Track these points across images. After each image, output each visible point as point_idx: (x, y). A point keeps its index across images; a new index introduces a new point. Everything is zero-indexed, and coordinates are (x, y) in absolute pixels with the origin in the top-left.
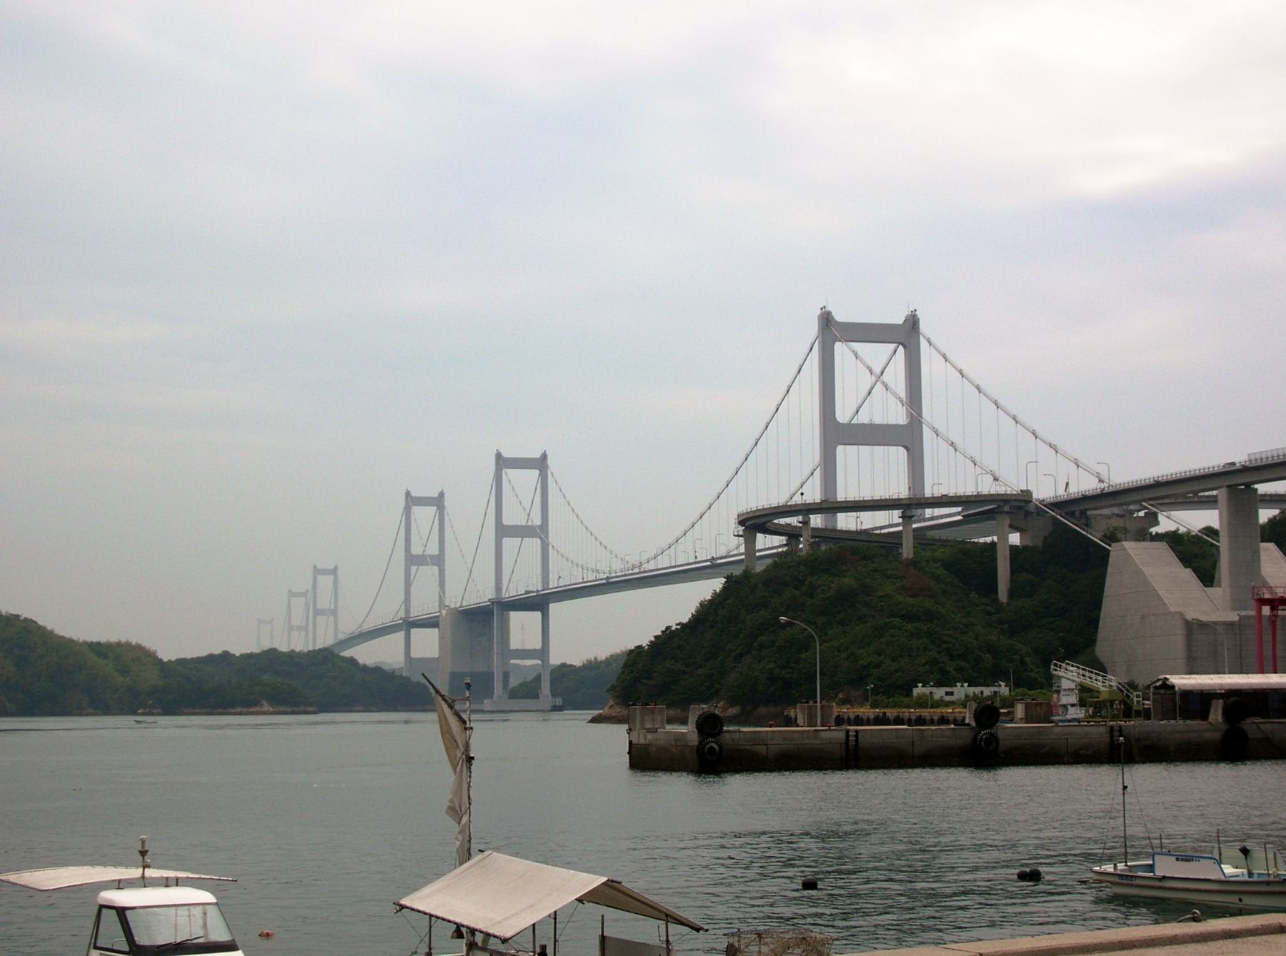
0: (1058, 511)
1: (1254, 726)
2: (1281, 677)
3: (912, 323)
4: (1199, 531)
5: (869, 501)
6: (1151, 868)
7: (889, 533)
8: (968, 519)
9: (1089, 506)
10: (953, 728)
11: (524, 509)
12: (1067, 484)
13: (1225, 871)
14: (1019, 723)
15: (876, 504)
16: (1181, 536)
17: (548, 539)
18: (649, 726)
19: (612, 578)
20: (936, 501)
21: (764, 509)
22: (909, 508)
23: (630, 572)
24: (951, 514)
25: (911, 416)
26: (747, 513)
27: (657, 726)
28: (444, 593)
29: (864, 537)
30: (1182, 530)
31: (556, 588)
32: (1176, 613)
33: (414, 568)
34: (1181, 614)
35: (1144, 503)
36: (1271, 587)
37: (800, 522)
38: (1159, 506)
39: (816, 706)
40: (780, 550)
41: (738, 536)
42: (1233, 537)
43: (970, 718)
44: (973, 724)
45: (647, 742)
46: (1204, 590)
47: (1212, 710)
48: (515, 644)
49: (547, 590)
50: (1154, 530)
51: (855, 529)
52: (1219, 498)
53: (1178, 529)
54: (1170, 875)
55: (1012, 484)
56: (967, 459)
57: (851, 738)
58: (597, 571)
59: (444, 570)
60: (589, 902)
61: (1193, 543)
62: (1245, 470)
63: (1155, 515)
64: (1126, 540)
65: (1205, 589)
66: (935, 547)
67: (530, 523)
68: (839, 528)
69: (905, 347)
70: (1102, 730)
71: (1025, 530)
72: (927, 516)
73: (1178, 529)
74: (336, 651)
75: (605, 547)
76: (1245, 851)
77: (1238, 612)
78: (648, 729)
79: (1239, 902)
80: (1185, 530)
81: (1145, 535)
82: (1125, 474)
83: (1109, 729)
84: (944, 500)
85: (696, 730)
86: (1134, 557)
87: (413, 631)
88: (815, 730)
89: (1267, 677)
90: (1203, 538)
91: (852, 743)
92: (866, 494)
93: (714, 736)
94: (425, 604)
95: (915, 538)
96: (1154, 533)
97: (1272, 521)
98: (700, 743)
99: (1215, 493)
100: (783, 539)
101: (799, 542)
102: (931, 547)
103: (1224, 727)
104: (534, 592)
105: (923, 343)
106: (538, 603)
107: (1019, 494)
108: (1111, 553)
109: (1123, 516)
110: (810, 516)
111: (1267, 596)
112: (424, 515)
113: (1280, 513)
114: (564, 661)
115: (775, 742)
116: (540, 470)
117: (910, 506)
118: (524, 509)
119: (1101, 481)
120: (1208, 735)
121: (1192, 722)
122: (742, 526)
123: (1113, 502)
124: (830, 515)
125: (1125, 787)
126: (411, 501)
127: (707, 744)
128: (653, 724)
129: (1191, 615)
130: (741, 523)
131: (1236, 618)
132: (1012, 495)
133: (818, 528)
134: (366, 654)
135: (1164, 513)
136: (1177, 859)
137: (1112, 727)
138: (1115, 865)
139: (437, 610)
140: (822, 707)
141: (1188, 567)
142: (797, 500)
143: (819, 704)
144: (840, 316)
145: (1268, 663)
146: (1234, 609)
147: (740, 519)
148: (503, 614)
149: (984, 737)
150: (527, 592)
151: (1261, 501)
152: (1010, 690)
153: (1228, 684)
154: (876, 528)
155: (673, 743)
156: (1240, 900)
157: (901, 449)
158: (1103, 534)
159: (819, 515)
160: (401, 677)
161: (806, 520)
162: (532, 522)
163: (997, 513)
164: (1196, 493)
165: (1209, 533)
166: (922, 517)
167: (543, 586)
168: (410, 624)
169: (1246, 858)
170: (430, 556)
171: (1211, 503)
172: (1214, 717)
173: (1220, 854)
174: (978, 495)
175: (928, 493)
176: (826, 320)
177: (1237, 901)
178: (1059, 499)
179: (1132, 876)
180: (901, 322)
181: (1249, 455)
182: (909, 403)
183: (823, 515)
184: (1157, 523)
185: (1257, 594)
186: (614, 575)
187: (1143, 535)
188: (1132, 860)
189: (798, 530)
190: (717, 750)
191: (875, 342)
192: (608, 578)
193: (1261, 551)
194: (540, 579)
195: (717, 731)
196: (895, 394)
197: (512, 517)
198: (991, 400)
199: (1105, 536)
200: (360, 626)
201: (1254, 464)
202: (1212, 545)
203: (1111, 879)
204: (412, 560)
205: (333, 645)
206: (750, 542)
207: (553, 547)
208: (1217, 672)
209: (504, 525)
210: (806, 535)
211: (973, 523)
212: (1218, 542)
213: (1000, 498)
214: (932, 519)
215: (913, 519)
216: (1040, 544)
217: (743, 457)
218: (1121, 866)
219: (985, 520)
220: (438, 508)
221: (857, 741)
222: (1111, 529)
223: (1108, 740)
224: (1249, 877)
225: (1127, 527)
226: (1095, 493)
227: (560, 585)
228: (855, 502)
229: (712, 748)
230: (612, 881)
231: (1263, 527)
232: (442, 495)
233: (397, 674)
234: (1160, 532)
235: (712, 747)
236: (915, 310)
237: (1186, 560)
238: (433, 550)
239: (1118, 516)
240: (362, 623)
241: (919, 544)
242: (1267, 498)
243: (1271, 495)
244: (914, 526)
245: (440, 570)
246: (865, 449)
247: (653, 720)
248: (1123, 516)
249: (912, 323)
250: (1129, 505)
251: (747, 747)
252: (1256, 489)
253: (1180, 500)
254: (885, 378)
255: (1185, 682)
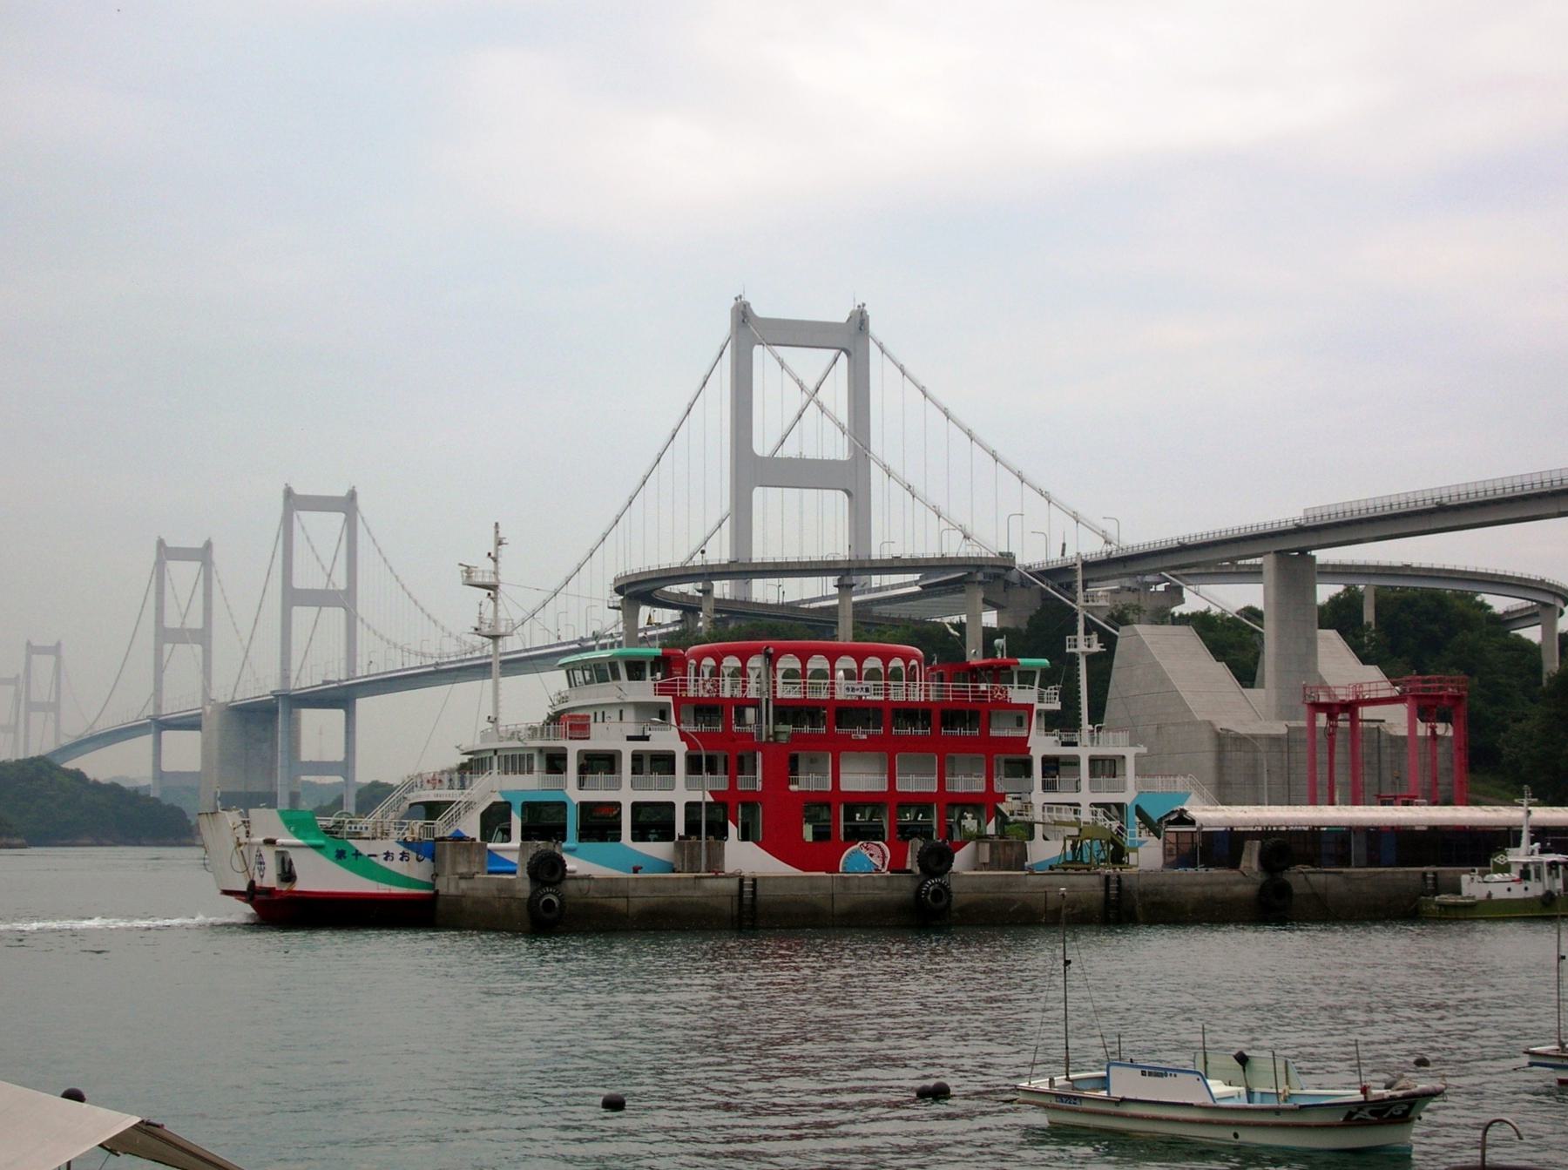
0: (1049, 582)
1: (1302, 878)
2: (1338, 810)
3: (860, 322)
4: (1237, 613)
5: (807, 562)
6: (1104, 1082)
7: (821, 608)
8: (928, 591)
9: (1093, 576)
10: (888, 877)
11: (323, 568)
12: (1064, 545)
13: (1214, 1090)
14: (981, 870)
15: (803, 568)
16: (1214, 618)
17: (355, 608)
18: (463, 869)
19: (443, 664)
20: (884, 565)
21: (650, 572)
22: (848, 574)
23: (469, 656)
24: (908, 583)
25: (853, 448)
26: (626, 576)
27: (475, 870)
28: (210, 684)
29: (786, 612)
30: (1215, 611)
31: (366, 677)
32: (1204, 721)
33: (168, 647)
34: (1210, 723)
35: (1163, 573)
36: (1329, 688)
37: (699, 591)
38: (1183, 578)
39: (700, 844)
40: (671, 629)
41: (614, 608)
42: (1281, 622)
43: (912, 861)
44: (917, 870)
45: (459, 893)
46: (1242, 693)
47: (1244, 856)
48: (308, 753)
49: (353, 679)
50: (1177, 610)
51: (776, 602)
52: (1265, 569)
53: (1209, 610)
54: (1133, 1097)
55: (989, 542)
56: (928, 510)
57: (746, 889)
58: (423, 655)
59: (210, 651)
60: (125, 1153)
61: (1229, 628)
62: (1299, 530)
63: (1179, 590)
64: (1139, 623)
65: (1244, 690)
66: (882, 628)
67: (331, 587)
68: (754, 600)
69: (848, 354)
70: (1094, 880)
71: (1003, 607)
72: (873, 586)
73: (1209, 610)
74: (57, 760)
75: (435, 622)
76: (1242, 1059)
77: (1287, 723)
78: (462, 874)
79: (1234, 1139)
80: (1219, 611)
81: (1166, 616)
82: (1138, 535)
83: (1103, 878)
84: (896, 564)
85: (527, 876)
86: (1149, 646)
87: (165, 734)
88: (696, 877)
89: (1320, 810)
90: (1242, 622)
91: (747, 896)
92: (791, 555)
93: (551, 884)
94: (181, 697)
95: (856, 614)
96: (1177, 615)
97: (1335, 601)
98: (533, 894)
99: (1259, 561)
100: (675, 614)
101: (697, 619)
102: (878, 627)
103: (1261, 878)
104: (334, 682)
105: (873, 348)
106: (340, 697)
107: (996, 558)
108: (1119, 640)
109: (1134, 590)
110: (714, 582)
111: (1323, 699)
112: (184, 574)
113: (1345, 590)
114: (374, 779)
115: (639, 893)
116: (346, 514)
117: (847, 572)
118: (323, 568)
119: (1108, 542)
120: (1240, 889)
121: (1216, 872)
122: (621, 594)
123: (1123, 571)
124: (741, 582)
125: (1067, 963)
126: (165, 553)
127: (542, 896)
128: (469, 868)
129: (1223, 723)
130: (619, 590)
131: (1284, 731)
132: (987, 558)
133: (724, 599)
134: (99, 767)
135: (1190, 587)
136: (1143, 1073)
137: (1107, 877)
138: (1051, 1081)
139: (200, 706)
140: (708, 845)
141: (1221, 661)
142: (698, 560)
143: (703, 841)
144: (761, 310)
145: (1322, 791)
146: (1280, 716)
147: (617, 585)
148: (290, 713)
149: (931, 888)
150: (326, 683)
151: (1319, 573)
152: (979, 824)
153: (1266, 819)
154: (803, 601)
155: (496, 893)
156: (1236, 1136)
157: (841, 494)
158: (1108, 613)
159: (728, 582)
160: (147, 798)
161: (708, 587)
162: (334, 584)
163: (966, 583)
164: (1233, 560)
165: (1250, 615)
166: (867, 587)
167: (348, 674)
168: (162, 725)
169: (1244, 1070)
170: (190, 630)
171: (1254, 574)
172: (1247, 864)
173: (1206, 1063)
174: (943, 558)
175: (875, 555)
176: (743, 315)
177: (1232, 1136)
178: (1050, 566)
179: (1075, 1098)
180: (844, 320)
181: (1306, 510)
182: (852, 431)
183: (733, 581)
184: (1182, 601)
185: (1310, 696)
186: (446, 660)
187: (1162, 617)
188: (1076, 1071)
189: (697, 601)
190: (557, 905)
191: (822, 347)
192: (437, 664)
193: (1319, 641)
194: (343, 664)
195: (557, 877)
196: (834, 420)
197: (307, 577)
198: (941, 409)
199: (1112, 616)
200: (91, 727)
201: (1311, 523)
202: (1254, 631)
203: (1046, 1100)
204: (165, 635)
205: (54, 753)
206: (631, 617)
207: (362, 620)
208: (1257, 802)
209: (293, 589)
210: (708, 607)
211: (935, 596)
212: (1262, 627)
213: (972, 562)
214: (880, 589)
215: (854, 589)
216: (1024, 626)
217: (626, 501)
218: (1060, 1080)
219: (951, 593)
220: (204, 564)
221: (754, 893)
222: (1121, 607)
223: (1102, 894)
224: (1249, 1102)
225: (1141, 605)
226: (1099, 558)
227: (371, 673)
228: (776, 564)
229: (550, 901)
230: (148, 1124)
231: (1322, 609)
232: (208, 546)
233: (142, 793)
234: (1185, 613)
235: (550, 901)
236: (864, 305)
237: (1219, 651)
238: (195, 621)
239: (1129, 589)
240: (95, 722)
241: (862, 623)
242: (1329, 570)
243: (1334, 566)
244: (854, 599)
245: (204, 651)
246: (791, 494)
247: (469, 862)
248: (1134, 590)
249: (860, 322)
250: (1144, 575)
251: (600, 900)
252: (1314, 557)
253: (1213, 570)
254: (821, 395)
255: (1209, 815)
